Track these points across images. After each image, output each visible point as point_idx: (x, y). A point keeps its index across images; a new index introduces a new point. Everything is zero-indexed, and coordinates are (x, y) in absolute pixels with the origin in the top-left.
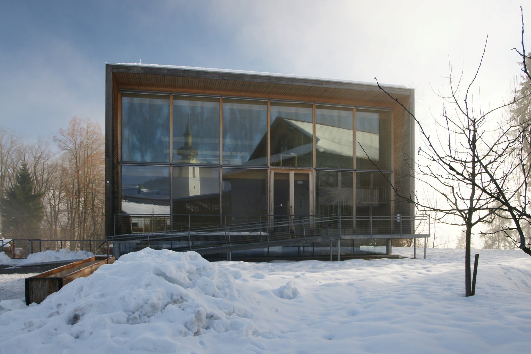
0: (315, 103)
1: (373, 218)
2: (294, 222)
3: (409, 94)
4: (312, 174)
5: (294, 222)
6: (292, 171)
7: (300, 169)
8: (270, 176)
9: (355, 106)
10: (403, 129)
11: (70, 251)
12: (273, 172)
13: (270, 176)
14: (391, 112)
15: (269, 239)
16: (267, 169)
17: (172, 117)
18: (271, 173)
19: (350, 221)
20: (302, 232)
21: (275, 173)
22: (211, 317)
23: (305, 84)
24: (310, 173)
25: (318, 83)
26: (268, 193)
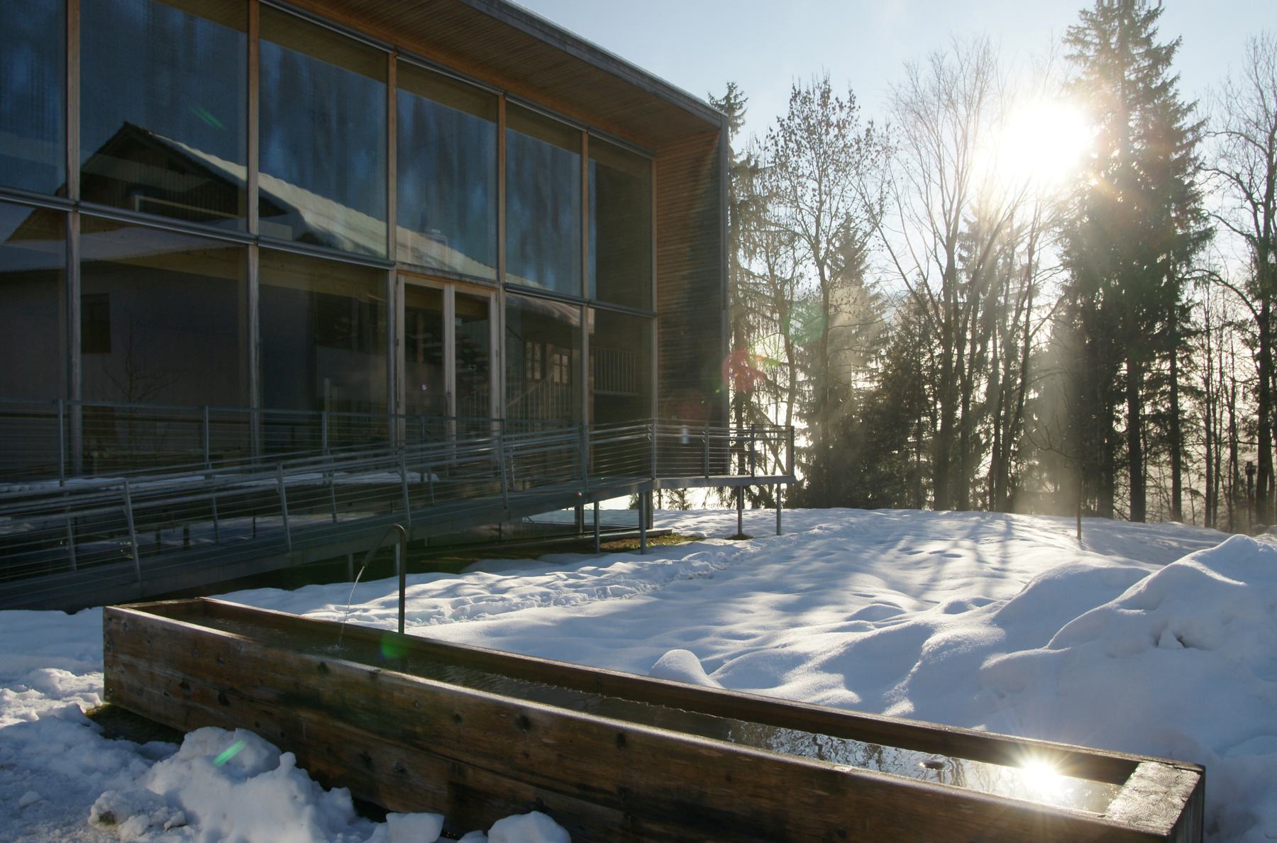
0: (505, 94)
1: (691, 432)
2: (458, 445)
3: (718, 124)
4: (497, 300)
5: (458, 445)
6: (449, 283)
7: (470, 283)
8: (395, 293)
9: (588, 128)
10: (694, 211)
11: (977, 541)
12: (403, 280)
13: (395, 293)
14: (651, 160)
15: (288, 499)
16: (388, 271)
17: (78, 18)
18: (397, 282)
19: (640, 439)
20: (660, 468)
21: (407, 286)
22: (189, 820)
23: (528, 30)
24: (493, 296)
25: (557, 36)
26: (392, 346)
